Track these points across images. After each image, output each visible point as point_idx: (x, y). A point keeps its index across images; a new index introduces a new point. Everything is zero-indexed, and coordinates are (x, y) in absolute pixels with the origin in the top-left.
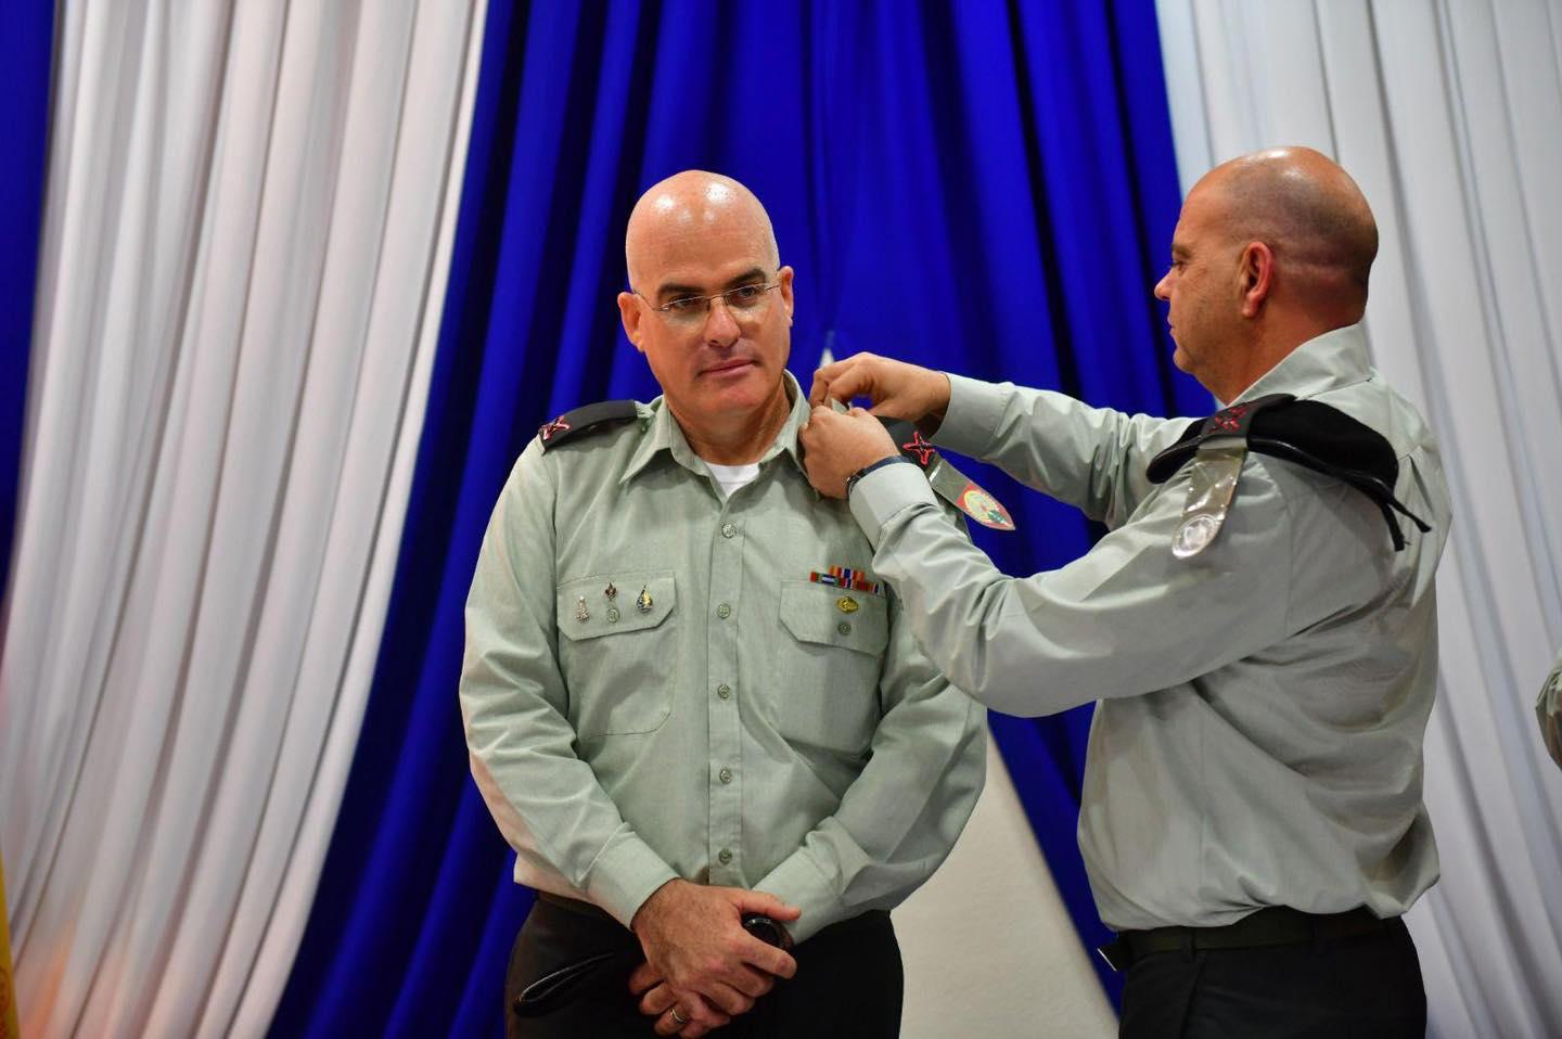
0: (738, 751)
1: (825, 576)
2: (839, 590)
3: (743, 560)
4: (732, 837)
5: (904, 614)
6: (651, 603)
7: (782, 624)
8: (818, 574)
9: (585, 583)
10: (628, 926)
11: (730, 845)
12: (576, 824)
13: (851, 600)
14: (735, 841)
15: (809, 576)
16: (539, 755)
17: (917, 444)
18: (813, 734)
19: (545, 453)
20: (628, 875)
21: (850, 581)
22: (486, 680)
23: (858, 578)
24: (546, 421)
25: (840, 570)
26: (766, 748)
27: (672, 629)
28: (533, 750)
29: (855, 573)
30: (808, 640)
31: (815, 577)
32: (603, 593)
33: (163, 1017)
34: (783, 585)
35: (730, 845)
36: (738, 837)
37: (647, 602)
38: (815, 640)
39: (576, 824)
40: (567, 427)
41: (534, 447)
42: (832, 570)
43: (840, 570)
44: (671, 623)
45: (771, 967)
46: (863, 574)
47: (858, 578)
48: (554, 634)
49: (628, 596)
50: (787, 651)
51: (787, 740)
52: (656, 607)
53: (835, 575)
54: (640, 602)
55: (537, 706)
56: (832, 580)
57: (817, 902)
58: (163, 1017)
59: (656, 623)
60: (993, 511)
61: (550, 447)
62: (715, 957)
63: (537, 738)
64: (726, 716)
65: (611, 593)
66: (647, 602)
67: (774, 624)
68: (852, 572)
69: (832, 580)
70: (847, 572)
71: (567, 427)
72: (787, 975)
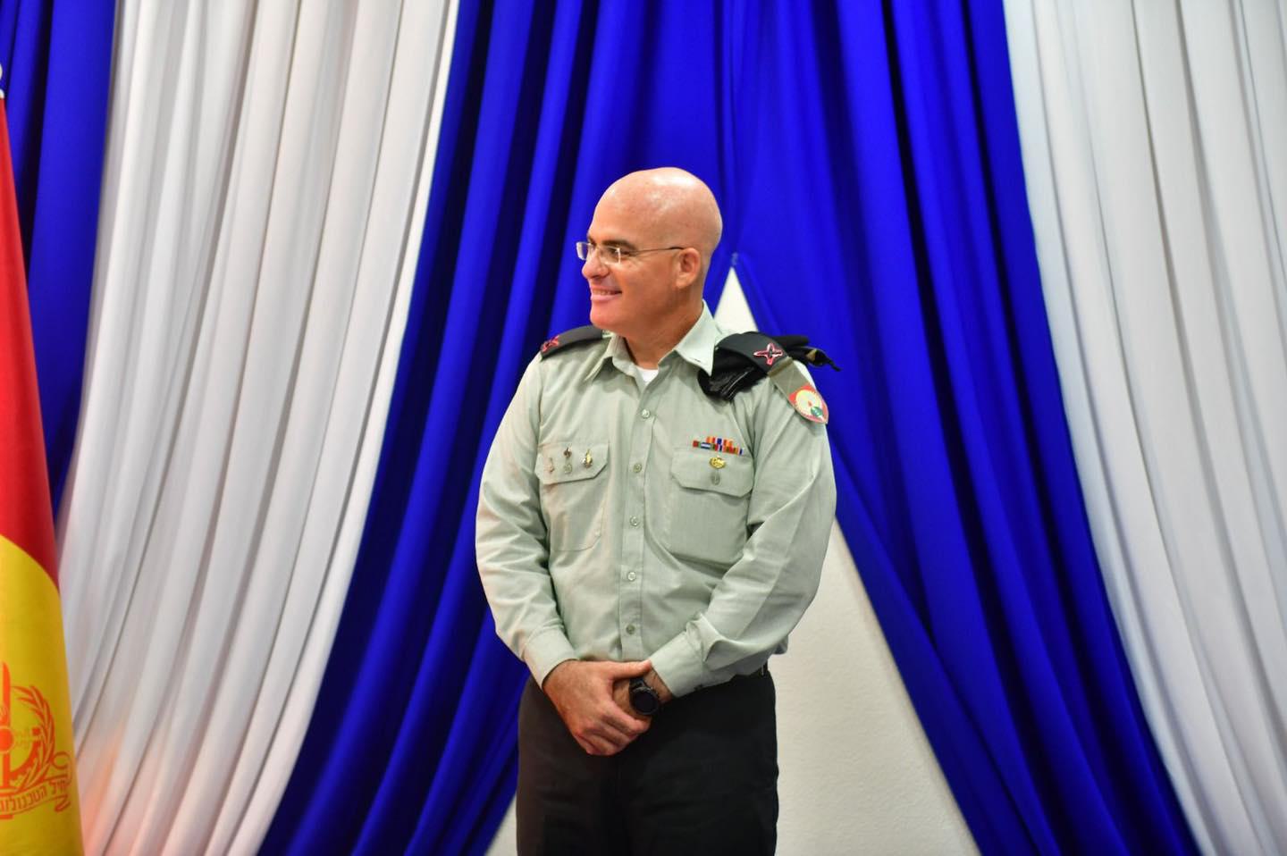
0: (641, 559)
4: (634, 617)
5: (730, 504)
6: (591, 462)
7: (672, 477)
10: (540, 683)
11: (633, 622)
12: (519, 619)
14: (637, 619)
15: (692, 444)
16: (508, 570)
20: (543, 651)
21: (721, 447)
22: (489, 515)
23: (727, 445)
24: (546, 340)
25: (714, 439)
27: (603, 480)
28: (504, 566)
29: (725, 441)
30: (689, 486)
31: (696, 444)
32: (563, 454)
33: (176, 839)
35: (633, 622)
36: (638, 616)
38: (693, 486)
39: (519, 619)
41: (538, 357)
42: (708, 439)
43: (714, 439)
44: (604, 474)
47: (727, 445)
48: (535, 484)
49: (579, 456)
50: (676, 494)
51: (674, 554)
52: (594, 464)
53: (711, 442)
55: (513, 532)
57: (686, 665)
58: (176, 839)
59: (594, 475)
60: (817, 408)
61: (545, 357)
62: (590, 720)
63: (511, 556)
64: (634, 539)
66: (588, 461)
67: (667, 476)
70: (720, 441)
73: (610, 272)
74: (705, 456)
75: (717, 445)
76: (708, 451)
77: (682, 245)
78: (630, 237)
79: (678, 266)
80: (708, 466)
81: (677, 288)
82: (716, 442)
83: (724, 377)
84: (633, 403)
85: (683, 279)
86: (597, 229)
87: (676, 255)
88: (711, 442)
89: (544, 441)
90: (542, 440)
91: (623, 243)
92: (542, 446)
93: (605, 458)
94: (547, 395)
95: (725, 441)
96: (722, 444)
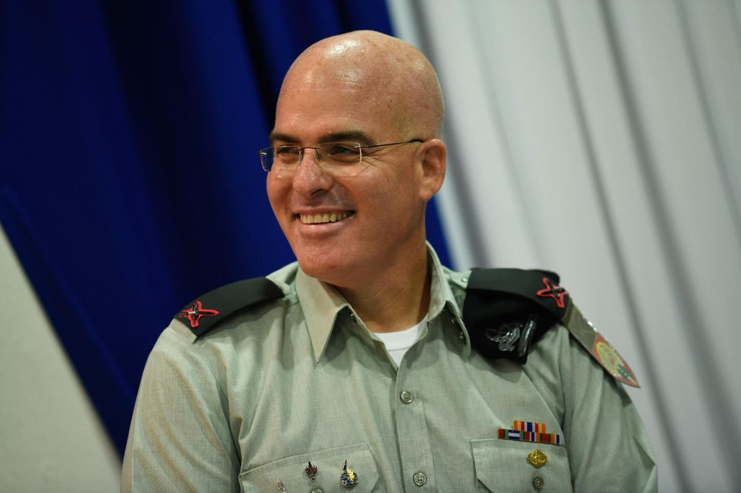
1: (510, 431)
2: (525, 444)
3: (426, 418)
8: (504, 430)
9: (278, 465)
13: (539, 452)
15: (497, 434)
17: (549, 288)
18: (523, 374)
19: (195, 341)
21: (533, 434)
26: (351, 177)
29: (537, 426)
31: (502, 434)
34: (472, 445)
37: (352, 477)
40: (216, 312)
42: (516, 423)
43: (523, 424)
45: (520, 349)
46: (544, 426)
47: (540, 431)
53: (519, 429)
54: (345, 476)
56: (517, 435)
65: (311, 471)
66: (352, 477)
68: (534, 425)
69: (517, 435)
71: (216, 312)
72: (327, 488)
73: (335, 181)
74: (521, 451)
75: (527, 433)
76: (518, 443)
77: (424, 136)
78: (344, 122)
79: (419, 168)
80: (528, 465)
81: (421, 199)
82: (526, 430)
83: (529, 325)
84: (382, 386)
85: (427, 186)
86: (290, 119)
87: (417, 149)
88: (519, 429)
89: (255, 460)
90: (248, 457)
91: (358, 136)
92: (251, 467)
93: (374, 469)
94: (238, 389)
95: (537, 426)
96: (534, 430)
